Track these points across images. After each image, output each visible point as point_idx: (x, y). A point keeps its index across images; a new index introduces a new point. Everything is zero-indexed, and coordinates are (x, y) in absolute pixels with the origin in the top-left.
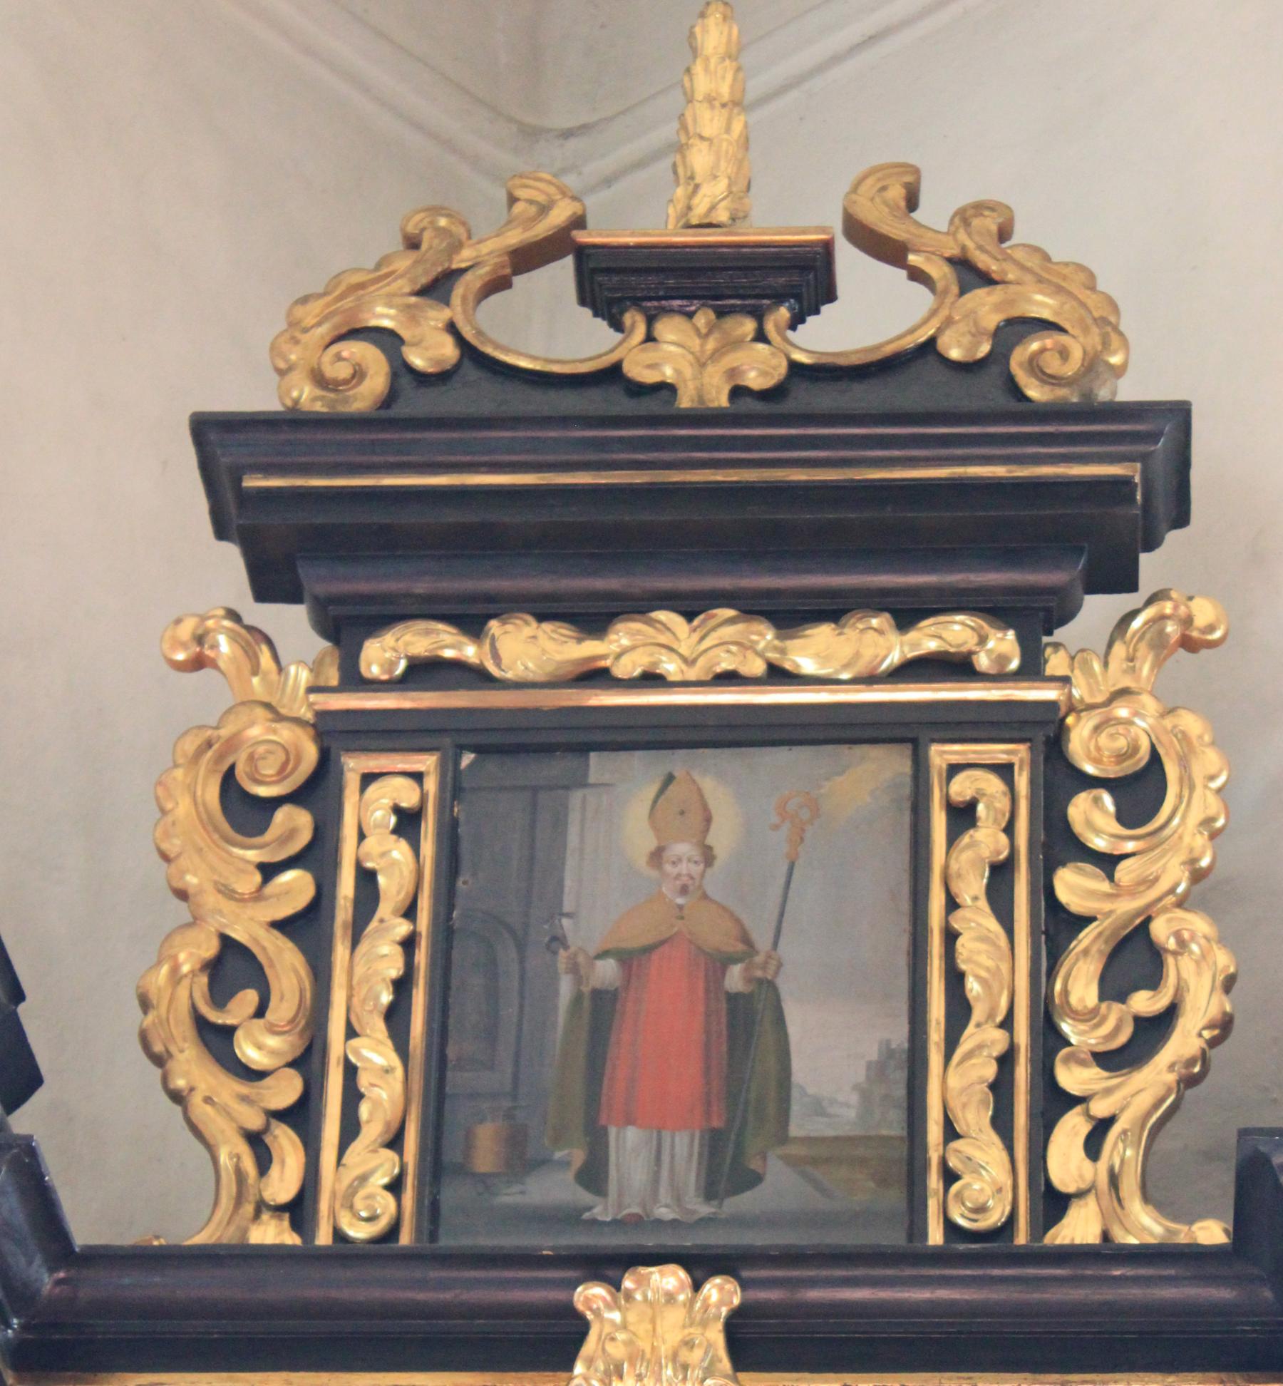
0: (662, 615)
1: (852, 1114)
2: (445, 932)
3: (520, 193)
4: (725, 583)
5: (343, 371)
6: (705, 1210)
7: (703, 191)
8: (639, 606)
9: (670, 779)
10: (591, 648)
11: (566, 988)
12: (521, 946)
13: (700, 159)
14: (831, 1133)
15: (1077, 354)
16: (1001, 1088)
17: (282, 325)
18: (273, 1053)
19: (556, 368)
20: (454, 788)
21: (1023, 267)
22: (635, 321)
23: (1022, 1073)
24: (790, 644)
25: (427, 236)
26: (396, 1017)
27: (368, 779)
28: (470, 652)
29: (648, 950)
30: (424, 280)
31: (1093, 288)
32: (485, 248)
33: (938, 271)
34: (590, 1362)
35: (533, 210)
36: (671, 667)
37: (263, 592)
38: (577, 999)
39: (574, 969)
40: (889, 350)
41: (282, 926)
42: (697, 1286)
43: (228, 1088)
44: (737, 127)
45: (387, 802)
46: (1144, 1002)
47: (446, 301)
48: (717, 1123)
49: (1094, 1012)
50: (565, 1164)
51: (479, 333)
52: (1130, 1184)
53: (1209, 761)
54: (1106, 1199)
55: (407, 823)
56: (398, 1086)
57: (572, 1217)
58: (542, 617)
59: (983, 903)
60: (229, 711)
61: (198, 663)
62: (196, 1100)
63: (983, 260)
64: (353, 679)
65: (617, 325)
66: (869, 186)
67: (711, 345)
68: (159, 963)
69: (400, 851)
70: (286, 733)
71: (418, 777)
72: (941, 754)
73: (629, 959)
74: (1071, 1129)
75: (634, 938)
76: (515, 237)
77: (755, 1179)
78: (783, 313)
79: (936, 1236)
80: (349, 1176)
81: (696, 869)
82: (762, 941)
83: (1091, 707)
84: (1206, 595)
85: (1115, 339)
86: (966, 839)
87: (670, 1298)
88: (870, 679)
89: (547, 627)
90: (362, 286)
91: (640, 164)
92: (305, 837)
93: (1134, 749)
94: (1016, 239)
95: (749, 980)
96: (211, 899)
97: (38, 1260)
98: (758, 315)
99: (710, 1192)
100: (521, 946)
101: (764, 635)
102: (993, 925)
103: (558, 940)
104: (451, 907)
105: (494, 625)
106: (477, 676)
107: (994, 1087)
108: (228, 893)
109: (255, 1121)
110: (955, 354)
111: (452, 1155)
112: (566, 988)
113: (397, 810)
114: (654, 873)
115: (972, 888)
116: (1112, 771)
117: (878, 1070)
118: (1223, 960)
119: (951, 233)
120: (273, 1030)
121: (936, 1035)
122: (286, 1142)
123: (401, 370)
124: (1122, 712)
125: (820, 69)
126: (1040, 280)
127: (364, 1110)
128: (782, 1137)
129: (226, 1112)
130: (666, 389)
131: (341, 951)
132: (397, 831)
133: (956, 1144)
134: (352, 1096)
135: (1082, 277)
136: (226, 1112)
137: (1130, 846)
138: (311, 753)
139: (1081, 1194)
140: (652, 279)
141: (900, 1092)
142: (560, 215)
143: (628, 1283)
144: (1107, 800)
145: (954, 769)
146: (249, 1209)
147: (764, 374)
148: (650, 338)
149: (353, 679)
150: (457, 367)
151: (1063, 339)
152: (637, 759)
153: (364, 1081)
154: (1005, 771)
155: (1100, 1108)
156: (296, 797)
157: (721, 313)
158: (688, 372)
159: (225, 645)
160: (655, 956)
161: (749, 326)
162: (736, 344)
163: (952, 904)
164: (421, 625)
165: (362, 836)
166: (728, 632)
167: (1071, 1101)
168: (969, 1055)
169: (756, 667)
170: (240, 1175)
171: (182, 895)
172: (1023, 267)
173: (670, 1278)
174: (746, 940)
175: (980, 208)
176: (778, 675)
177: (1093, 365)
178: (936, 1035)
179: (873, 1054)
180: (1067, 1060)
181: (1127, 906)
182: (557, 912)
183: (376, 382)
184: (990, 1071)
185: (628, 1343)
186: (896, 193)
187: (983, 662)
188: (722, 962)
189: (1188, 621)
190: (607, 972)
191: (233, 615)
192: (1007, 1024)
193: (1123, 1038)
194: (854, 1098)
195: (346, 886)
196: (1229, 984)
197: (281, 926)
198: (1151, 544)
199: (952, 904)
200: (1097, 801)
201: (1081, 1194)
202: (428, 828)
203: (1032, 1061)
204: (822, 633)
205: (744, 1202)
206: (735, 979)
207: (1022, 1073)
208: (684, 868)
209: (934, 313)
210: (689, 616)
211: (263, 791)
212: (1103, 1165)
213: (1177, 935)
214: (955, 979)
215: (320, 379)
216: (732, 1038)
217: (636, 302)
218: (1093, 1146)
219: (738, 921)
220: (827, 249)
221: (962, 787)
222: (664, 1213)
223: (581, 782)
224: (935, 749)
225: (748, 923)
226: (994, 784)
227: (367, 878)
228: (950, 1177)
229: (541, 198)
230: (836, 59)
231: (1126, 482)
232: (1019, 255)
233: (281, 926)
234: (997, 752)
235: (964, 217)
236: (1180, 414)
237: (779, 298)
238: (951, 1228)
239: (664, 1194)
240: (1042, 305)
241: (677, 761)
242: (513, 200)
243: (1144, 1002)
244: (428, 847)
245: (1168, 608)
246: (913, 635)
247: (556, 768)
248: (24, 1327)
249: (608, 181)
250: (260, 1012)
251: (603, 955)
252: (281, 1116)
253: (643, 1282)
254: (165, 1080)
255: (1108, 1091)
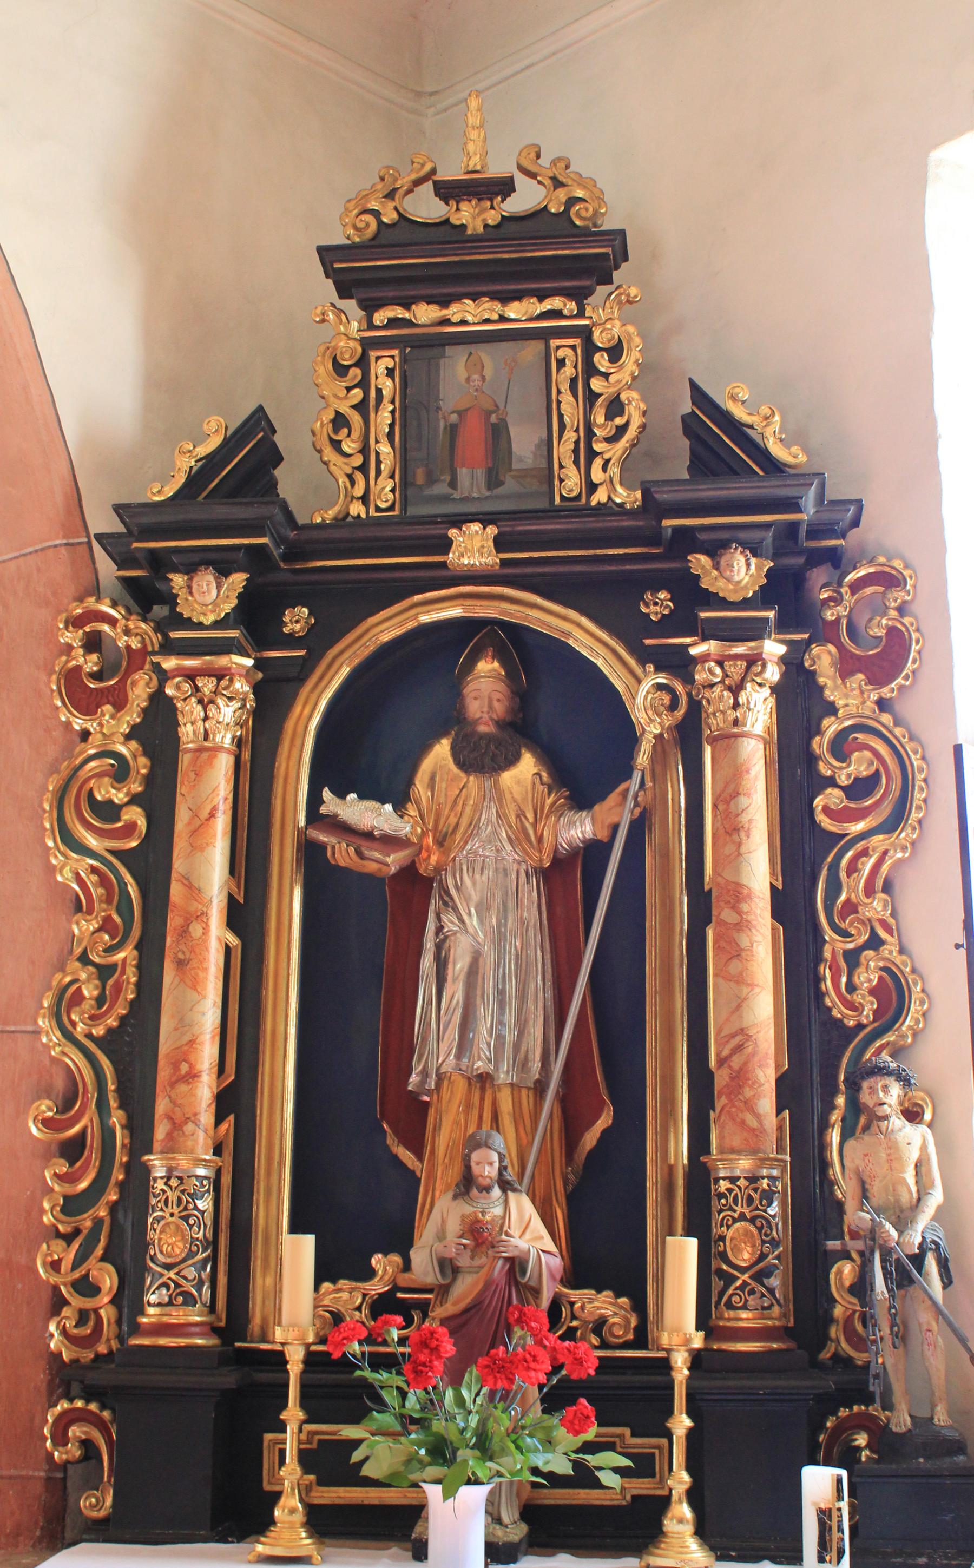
0: (466, 301)
1: (530, 461)
2: (404, 408)
3: (416, 160)
4: (484, 289)
5: (362, 225)
6: (488, 494)
7: (473, 159)
8: (458, 298)
9: (471, 354)
10: (445, 312)
11: (442, 424)
12: (427, 411)
13: (471, 147)
14: (525, 467)
15: (591, 210)
16: (576, 451)
17: (343, 210)
18: (353, 449)
19: (429, 221)
20: (404, 359)
21: (574, 180)
22: (453, 203)
23: (582, 445)
24: (506, 309)
25: (386, 177)
26: (390, 436)
27: (378, 358)
28: (407, 315)
29: (467, 410)
30: (386, 193)
31: (595, 186)
32: (405, 180)
33: (547, 182)
34: (454, 553)
35: (419, 166)
36: (469, 318)
37: (342, 296)
38: (445, 428)
39: (444, 418)
40: (533, 210)
41: (354, 407)
42: (484, 528)
43: (340, 460)
44: (482, 135)
45: (384, 366)
46: (619, 421)
47: (393, 199)
48: (490, 465)
49: (603, 425)
50: (444, 481)
51: (405, 210)
52: (616, 480)
53: (637, 340)
54: (609, 485)
55: (390, 373)
56: (392, 459)
57: (446, 499)
58: (428, 303)
59: (568, 391)
60: (334, 337)
61: (323, 321)
62: (331, 464)
63: (561, 178)
64: (371, 327)
65: (447, 204)
66: (524, 154)
67: (477, 211)
68: (317, 421)
69: (389, 383)
70: (352, 344)
71: (393, 357)
72: (554, 343)
73: (461, 414)
74: (598, 463)
75: (461, 407)
76: (414, 176)
77: (502, 483)
78: (499, 198)
79: (557, 500)
80: (379, 488)
81: (480, 383)
82: (502, 406)
83: (600, 324)
84: (634, 286)
85: (602, 204)
86: (562, 371)
87: (477, 532)
88: (530, 320)
89: (431, 306)
90: (367, 195)
91: (456, 104)
92: (359, 377)
93: (613, 337)
94: (572, 169)
95: (498, 419)
96: (332, 399)
97: (288, 529)
98: (491, 200)
99: (489, 488)
100: (427, 411)
101: (498, 306)
102: (572, 399)
103: (439, 408)
104: (405, 399)
105: (414, 307)
106: (408, 323)
107: (573, 451)
108: (336, 396)
109: (349, 471)
110: (553, 210)
111: (410, 479)
112: (442, 424)
113: (387, 368)
114: (465, 384)
115: (565, 387)
116: (606, 346)
117: (538, 447)
118: (643, 406)
119: (551, 168)
120: (353, 441)
121: (555, 435)
122: (359, 477)
123: (380, 223)
124: (609, 326)
125: (512, 76)
126: (579, 184)
127: (383, 467)
128: (510, 470)
129: (341, 468)
130: (463, 227)
131: (372, 415)
132: (387, 375)
133: (563, 470)
134: (379, 463)
135: (592, 183)
136: (341, 468)
137: (612, 370)
138: (359, 350)
139: (601, 484)
140: (457, 190)
141: (546, 453)
142: (428, 168)
143: (464, 529)
144: (605, 355)
145: (558, 347)
146: (349, 499)
147: (494, 220)
148: (458, 209)
149: (371, 327)
150: (398, 221)
151: (587, 205)
152: (460, 348)
153: (382, 458)
154: (573, 348)
155: (606, 456)
156: (355, 365)
157: (479, 200)
158: (470, 221)
159: (331, 316)
160: (469, 413)
161: (488, 204)
162: (484, 210)
163: (559, 392)
164: (390, 307)
165: (377, 377)
166: (487, 305)
167: (598, 454)
168: (566, 441)
169: (496, 317)
170: (346, 488)
171: (323, 397)
172: (574, 180)
173: (475, 527)
174: (497, 406)
175: (559, 159)
176: (503, 319)
177: (596, 213)
178: (555, 435)
179: (537, 441)
180: (596, 442)
181: (611, 390)
182: (437, 399)
183: (374, 226)
184: (572, 446)
185: (465, 547)
186: (533, 155)
187: (566, 312)
188: (489, 413)
189: (628, 295)
190: (454, 418)
191: (333, 305)
192: (577, 431)
193: (613, 432)
194: (531, 456)
195: (373, 394)
196: (644, 413)
197: (353, 407)
198: (617, 267)
199: (559, 392)
200: (602, 356)
201: (601, 484)
202: (397, 373)
203: (585, 442)
204: (516, 304)
205: (500, 491)
206: (493, 419)
207: (582, 445)
208: (476, 383)
209: (546, 197)
210: (474, 301)
211: (345, 363)
212: (607, 474)
213: (628, 399)
214: (561, 416)
215: (355, 228)
216: (493, 438)
217: (453, 197)
218: (604, 468)
219: (494, 401)
220: (511, 179)
221: (560, 354)
222: (475, 495)
223: (443, 356)
224: (552, 341)
225: (498, 401)
226: (569, 352)
227: (379, 391)
228: (561, 481)
229: (421, 161)
230: (517, 73)
231: (607, 254)
232: (572, 175)
233: (353, 407)
234: (571, 342)
235: (554, 162)
236: (622, 233)
237: (497, 194)
238: (562, 497)
239: (475, 489)
240: (580, 194)
241: (472, 348)
242: (413, 163)
243: (619, 421)
244: (397, 379)
245: (622, 290)
246: (544, 304)
247: (435, 351)
248: (285, 548)
249: (445, 110)
250: (349, 435)
251: (453, 412)
252: (358, 468)
253: (468, 528)
254: (321, 458)
255: (609, 450)
